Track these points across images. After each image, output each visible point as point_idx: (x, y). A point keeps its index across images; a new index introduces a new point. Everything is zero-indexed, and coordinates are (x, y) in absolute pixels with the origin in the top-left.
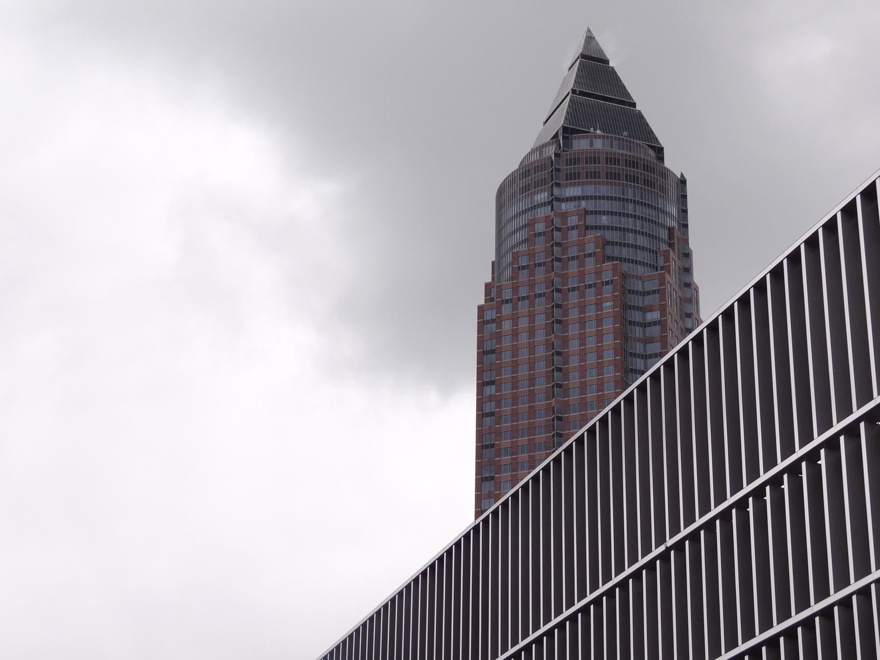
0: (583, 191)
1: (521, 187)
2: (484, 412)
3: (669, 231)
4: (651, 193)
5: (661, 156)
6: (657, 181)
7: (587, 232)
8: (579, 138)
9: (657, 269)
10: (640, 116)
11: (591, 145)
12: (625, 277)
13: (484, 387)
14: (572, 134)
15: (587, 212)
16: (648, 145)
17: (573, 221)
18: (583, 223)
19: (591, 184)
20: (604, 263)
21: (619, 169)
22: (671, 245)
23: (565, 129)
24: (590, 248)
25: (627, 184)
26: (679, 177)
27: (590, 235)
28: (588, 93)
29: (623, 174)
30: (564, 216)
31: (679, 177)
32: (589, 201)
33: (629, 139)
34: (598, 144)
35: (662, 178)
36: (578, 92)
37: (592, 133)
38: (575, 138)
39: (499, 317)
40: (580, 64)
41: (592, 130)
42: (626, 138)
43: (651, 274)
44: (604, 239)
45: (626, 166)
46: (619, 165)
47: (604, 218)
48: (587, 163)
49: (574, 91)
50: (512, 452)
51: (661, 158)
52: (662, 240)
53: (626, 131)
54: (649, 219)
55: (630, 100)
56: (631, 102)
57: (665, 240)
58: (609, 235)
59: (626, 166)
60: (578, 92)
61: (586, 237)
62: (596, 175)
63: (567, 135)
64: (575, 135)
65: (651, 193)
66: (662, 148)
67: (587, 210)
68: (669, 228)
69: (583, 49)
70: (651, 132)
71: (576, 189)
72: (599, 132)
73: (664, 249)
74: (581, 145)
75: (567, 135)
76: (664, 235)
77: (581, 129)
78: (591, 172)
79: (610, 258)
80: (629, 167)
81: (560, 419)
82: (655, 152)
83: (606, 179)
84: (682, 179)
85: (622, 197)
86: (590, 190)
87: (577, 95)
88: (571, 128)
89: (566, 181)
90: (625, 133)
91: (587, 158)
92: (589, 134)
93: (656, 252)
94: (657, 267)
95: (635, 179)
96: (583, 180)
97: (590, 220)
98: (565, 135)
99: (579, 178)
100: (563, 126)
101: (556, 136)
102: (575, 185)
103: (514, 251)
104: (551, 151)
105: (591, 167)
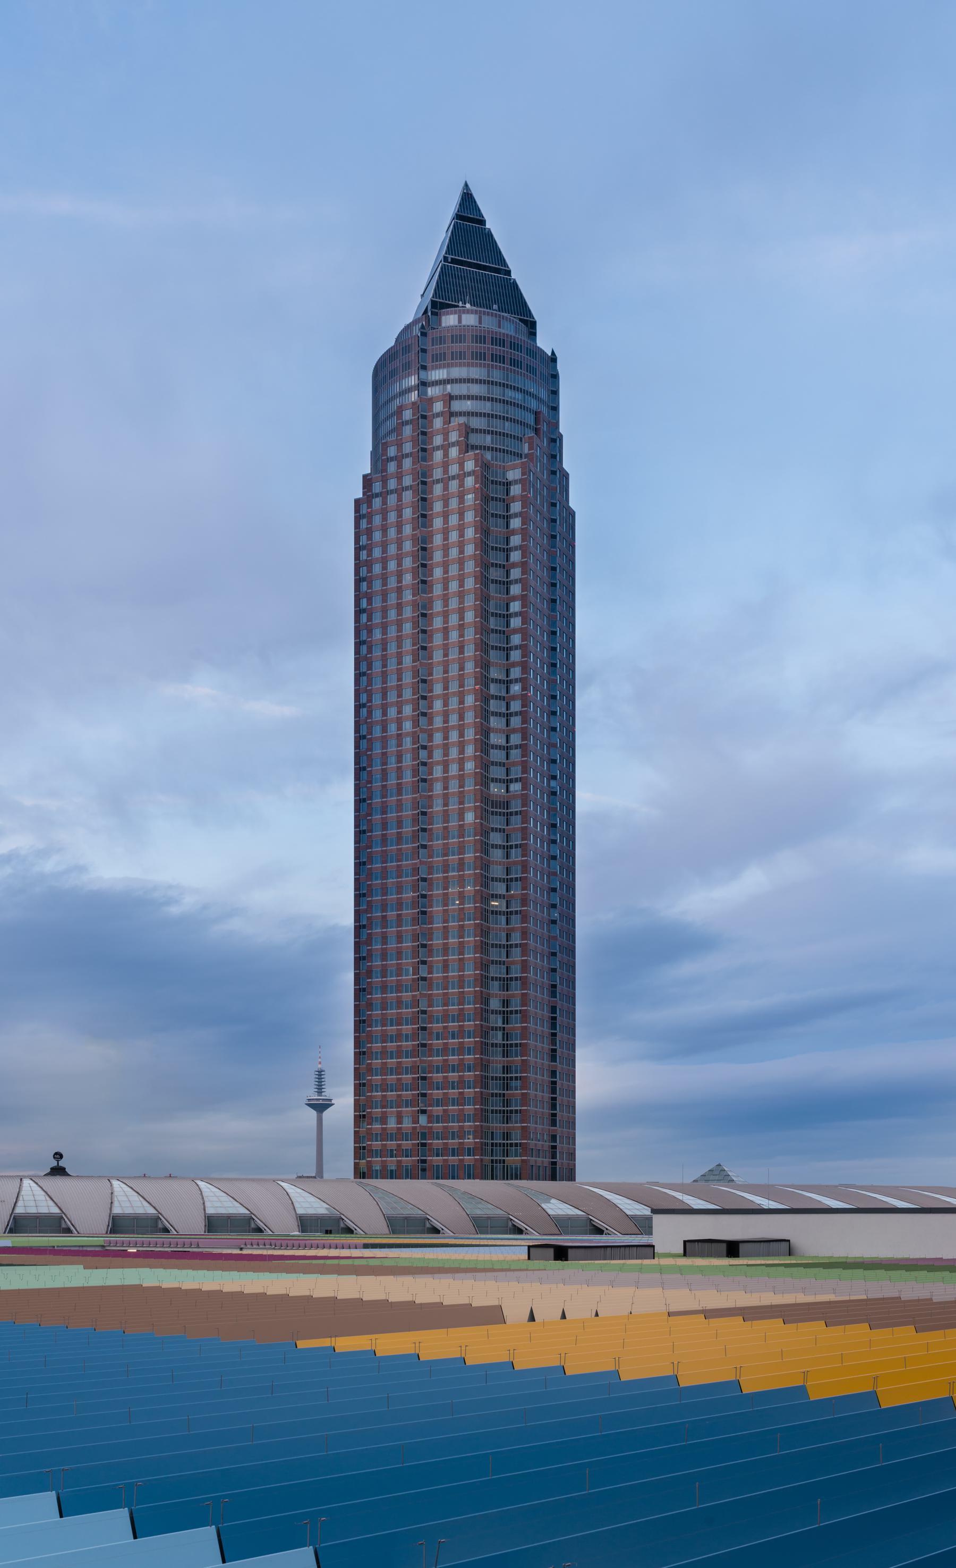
0: (448, 373)
1: (391, 370)
2: (361, 734)
3: (536, 414)
4: (518, 374)
5: (534, 331)
6: (524, 360)
7: (452, 419)
8: (448, 314)
9: (521, 457)
11: (460, 320)
12: (488, 467)
13: (361, 772)
14: (441, 308)
15: (451, 398)
16: (521, 320)
17: (438, 407)
18: (447, 409)
19: (476, 366)
20: (468, 452)
21: (484, 347)
22: (537, 431)
23: (434, 304)
24: (454, 437)
25: (492, 365)
26: (550, 354)
27: (456, 421)
28: (470, 262)
29: (489, 354)
30: (431, 401)
31: (550, 354)
32: (454, 385)
33: (498, 313)
34: (470, 320)
35: (530, 357)
36: (450, 260)
37: (461, 307)
38: (444, 315)
39: (368, 513)
40: (454, 226)
41: (460, 304)
42: (496, 312)
43: (515, 462)
44: (467, 426)
45: (492, 344)
46: (485, 343)
47: (469, 402)
48: (452, 342)
49: (445, 259)
50: (414, 901)
51: (533, 334)
52: (528, 426)
53: (496, 304)
54: (514, 403)
55: (505, 267)
56: (505, 270)
57: (530, 425)
58: (476, 423)
59: (492, 344)
60: (450, 260)
61: (450, 425)
62: (461, 355)
63: (436, 311)
64: (444, 310)
65: (518, 374)
66: (535, 322)
67: (452, 394)
68: (536, 412)
69: (460, 201)
70: (525, 304)
71: (441, 371)
72: (468, 306)
73: (530, 435)
74: (450, 320)
75: (436, 311)
76: (530, 419)
77: (450, 303)
78: (437, 354)
79: (474, 447)
80: (499, 346)
81: (424, 615)
82: (527, 326)
83: (472, 359)
84: (553, 357)
85: (506, 383)
86: (457, 372)
87: (449, 263)
88: (440, 302)
89: (432, 363)
90: (495, 307)
91: (452, 336)
92: (457, 309)
93: (521, 438)
94: (521, 455)
95: (502, 359)
96: (448, 362)
97: (457, 406)
98: (433, 310)
99: (445, 360)
100: (432, 301)
101: (426, 312)
102: (460, 365)
103: (383, 441)
104: (416, 331)
105: (457, 347)
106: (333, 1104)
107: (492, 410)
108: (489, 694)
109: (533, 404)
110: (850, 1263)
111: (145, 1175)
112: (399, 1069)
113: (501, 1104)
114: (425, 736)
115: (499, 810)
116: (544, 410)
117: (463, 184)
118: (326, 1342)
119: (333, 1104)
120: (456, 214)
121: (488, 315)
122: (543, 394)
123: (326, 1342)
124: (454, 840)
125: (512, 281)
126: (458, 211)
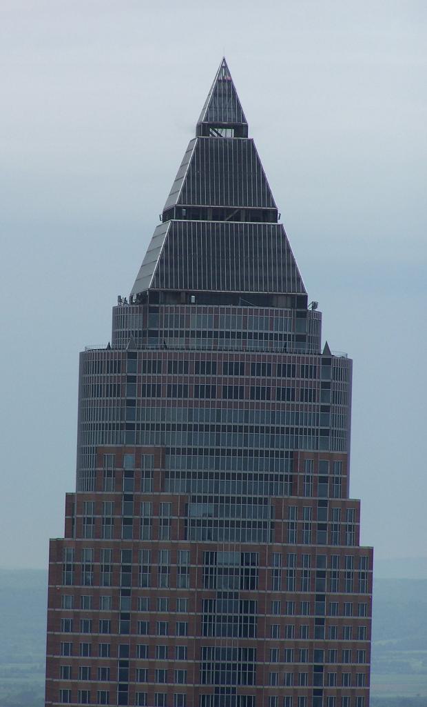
3: (291, 457)
10: (280, 234)
115: (230, 543)
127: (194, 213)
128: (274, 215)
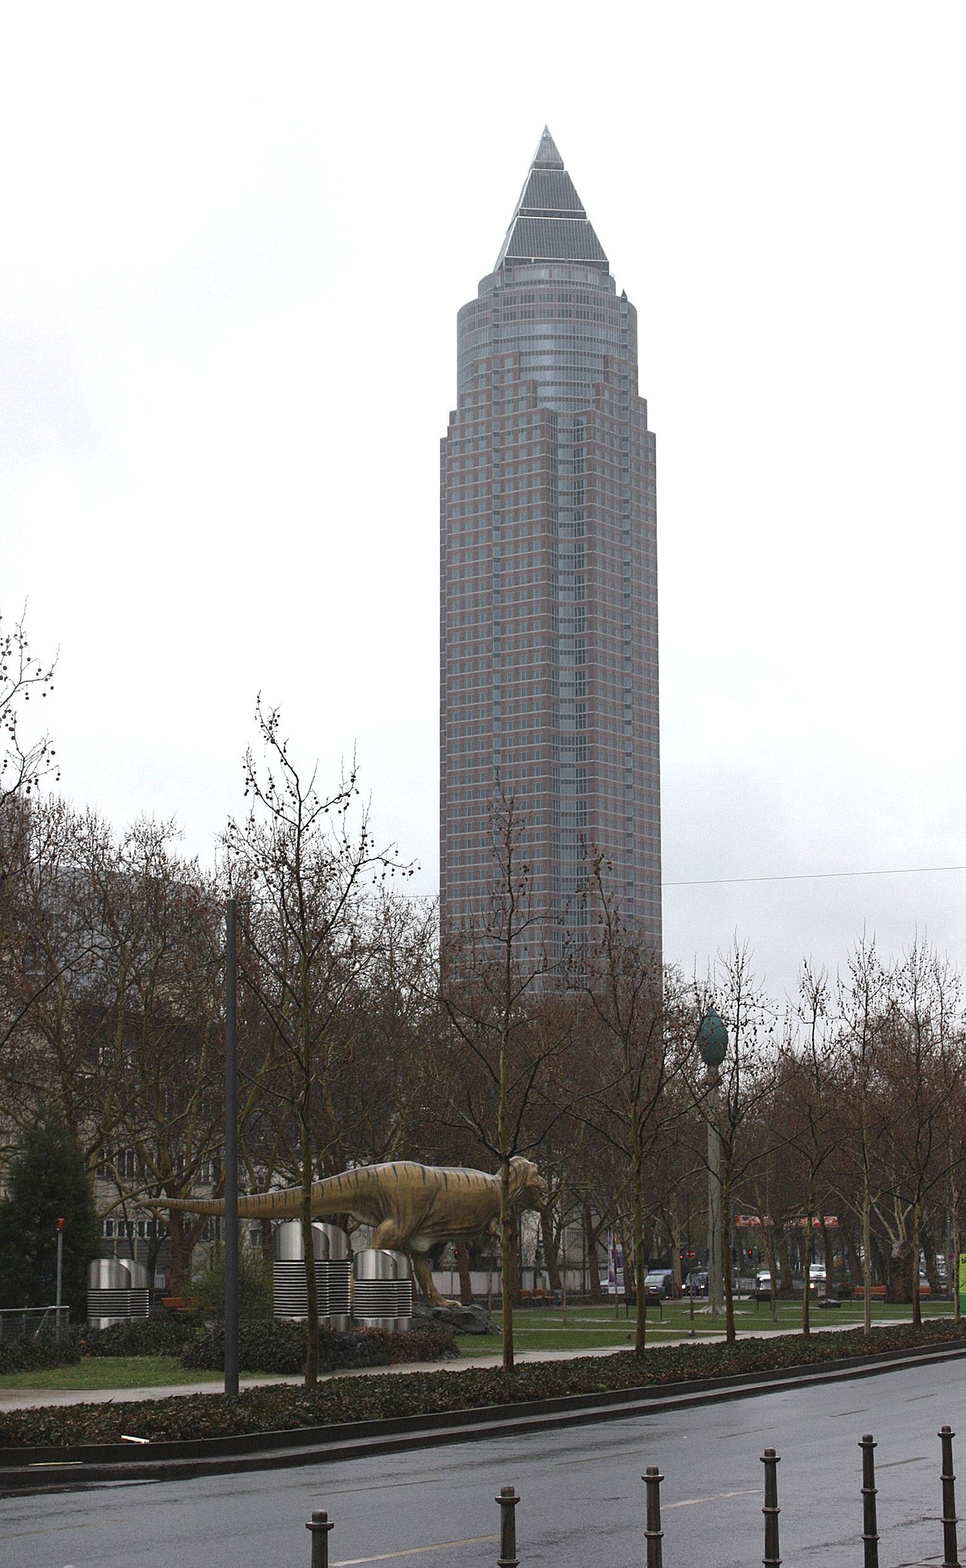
17: (509, 364)
26: (619, 294)
60: (525, 213)
66: (608, 263)
99: (515, 303)
106: (518, 1500)
107: (556, 363)
108: (556, 571)
109: (602, 350)
110: (670, 1407)
111: (385, 865)
112: (476, 776)
113: (574, 582)
114: (498, 548)
115: (568, 746)
116: (614, 353)
117: (543, 128)
118: (87, 1466)
119: (518, 1500)
120: (535, 163)
121: (558, 268)
122: (614, 338)
123: (87, 1466)
124: (511, 699)
125: (586, 223)
126: (537, 159)
127: (530, 213)
128: (584, 215)
